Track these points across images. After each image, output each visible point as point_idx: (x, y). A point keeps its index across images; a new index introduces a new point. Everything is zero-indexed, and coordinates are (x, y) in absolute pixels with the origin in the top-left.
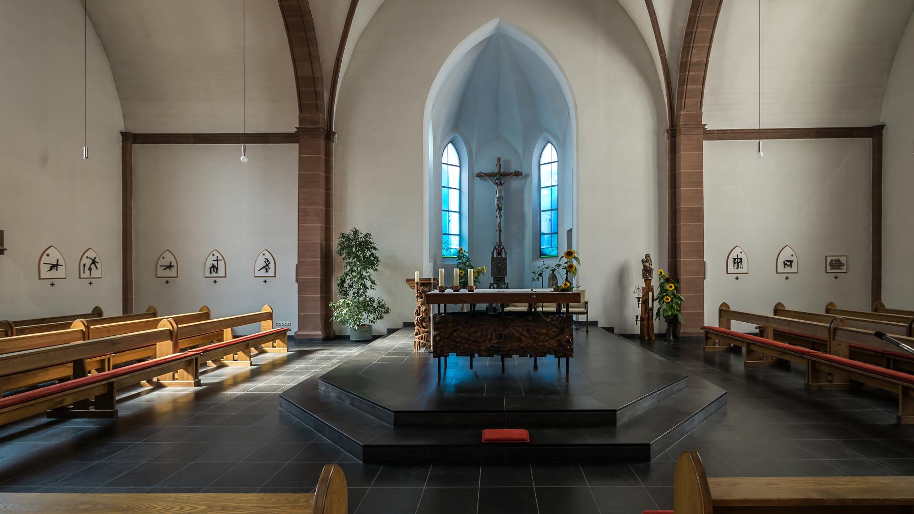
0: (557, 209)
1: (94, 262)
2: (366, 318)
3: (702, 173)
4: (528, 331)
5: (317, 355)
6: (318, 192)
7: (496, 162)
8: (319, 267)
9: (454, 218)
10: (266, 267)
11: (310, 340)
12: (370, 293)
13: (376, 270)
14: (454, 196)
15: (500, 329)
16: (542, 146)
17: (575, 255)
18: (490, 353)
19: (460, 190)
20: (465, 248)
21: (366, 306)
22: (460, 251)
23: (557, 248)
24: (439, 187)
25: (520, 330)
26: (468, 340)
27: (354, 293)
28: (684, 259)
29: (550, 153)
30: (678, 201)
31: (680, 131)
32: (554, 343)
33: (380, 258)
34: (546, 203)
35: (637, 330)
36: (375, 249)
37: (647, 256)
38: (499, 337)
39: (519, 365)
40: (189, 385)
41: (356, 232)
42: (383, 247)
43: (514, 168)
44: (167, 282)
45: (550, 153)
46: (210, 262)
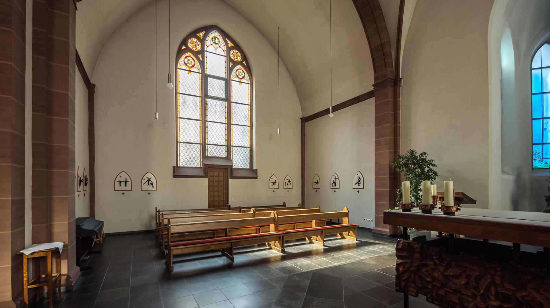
1: (289, 181)
8: (388, 182)
10: (358, 183)
11: (382, 235)
36: (433, 165)
40: (278, 251)
41: (412, 153)
44: (123, 194)
46: (333, 180)
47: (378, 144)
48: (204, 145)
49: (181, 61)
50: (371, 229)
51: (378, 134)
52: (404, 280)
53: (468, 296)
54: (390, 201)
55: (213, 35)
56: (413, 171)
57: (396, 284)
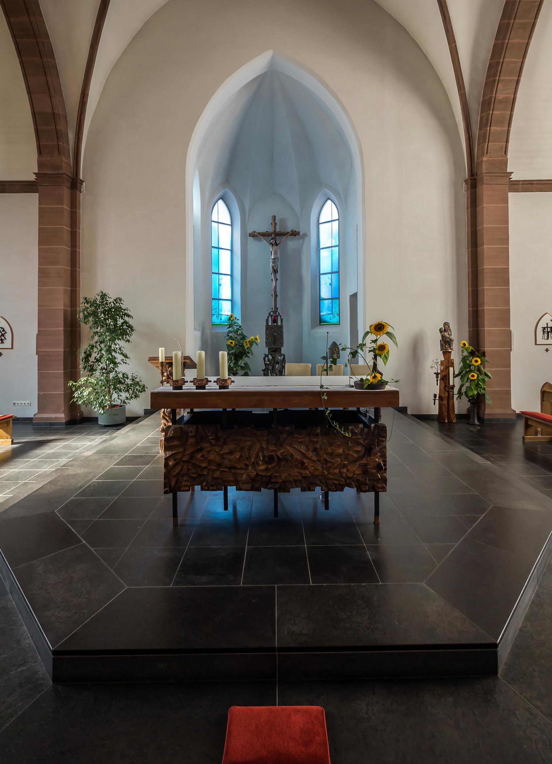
0: (338, 272)
2: (117, 398)
3: (507, 228)
4: (315, 450)
5: (47, 450)
6: (63, 246)
7: (271, 221)
9: (226, 281)
11: (51, 424)
12: (122, 368)
13: (128, 341)
14: (225, 259)
15: (271, 448)
16: (321, 203)
17: (389, 330)
18: (254, 485)
19: (232, 250)
20: (238, 315)
21: (117, 383)
22: (230, 318)
23: (339, 315)
24: (208, 249)
25: (303, 449)
26: (219, 465)
27: (102, 369)
28: (489, 328)
29: (329, 211)
30: (479, 262)
32: (355, 470)
33: (134, 328)
34: (326, 265)
35: (434, 410)
36: (128, 316)
37: (446, 324)
38: (270, 459)
39: (301, 501)
41: (104, 296)
42: (138, 312)
43: (290, 227)
45: (329, 211)
47: (43, 275)
50: (31, 419)
51: (44, 259)
52: (175, 476)
53: (241, 469)
54: (65, 368)
56: (103, 324)
57: (165, 484)
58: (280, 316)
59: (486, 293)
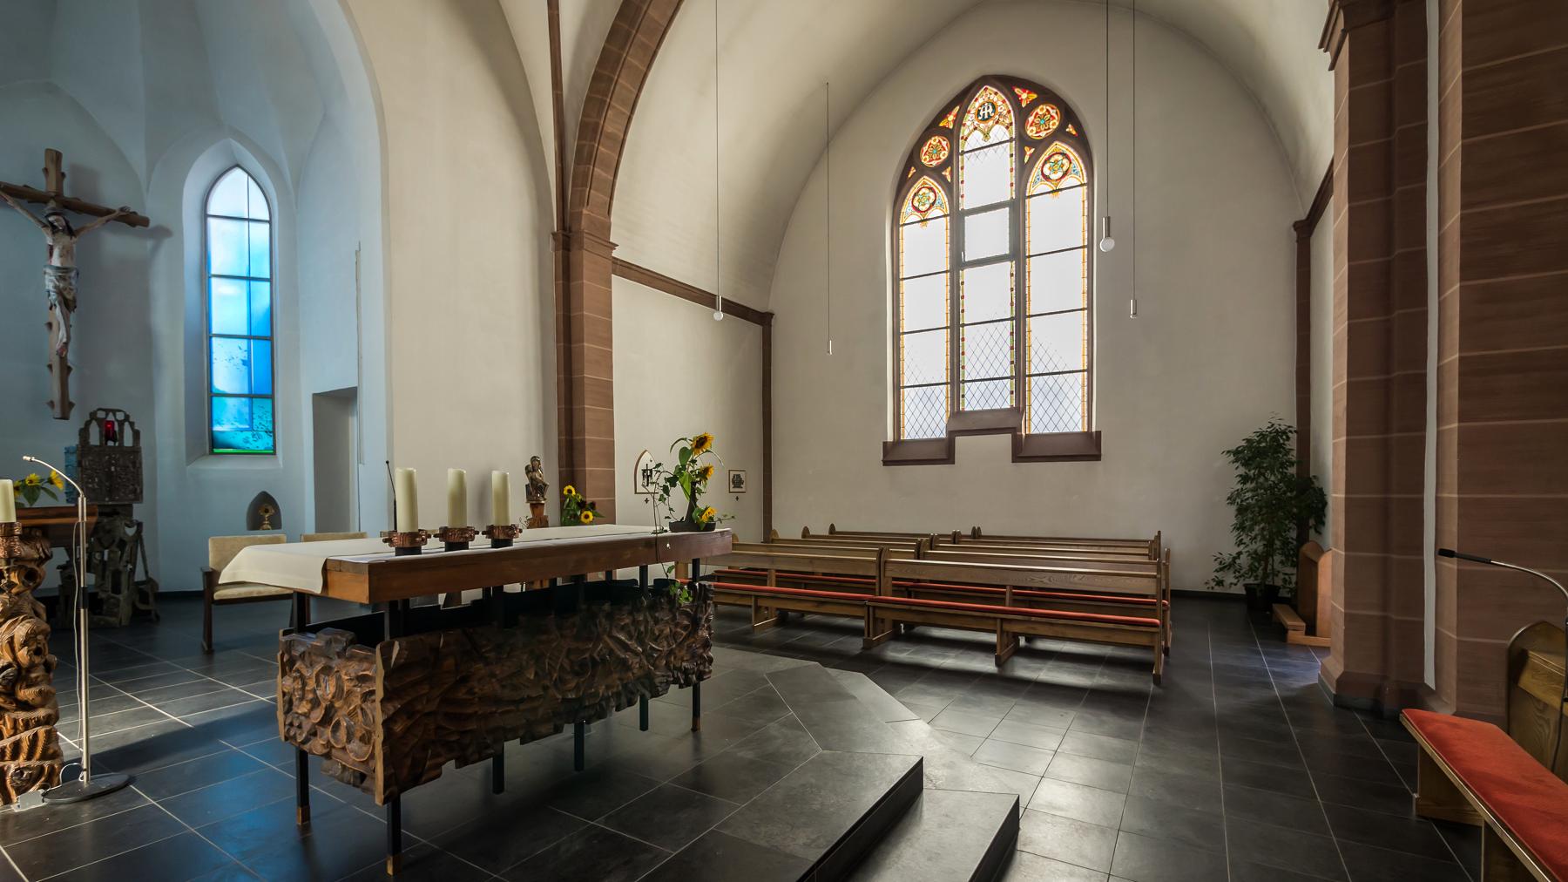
0: (270, 339)
31: (573, 243)
37: (534, 459)
43: (112, 195)
48: (955, 381)
49: (907, 208)
55: (994, 98)
58: (132, 424)
59: (588, 415)
